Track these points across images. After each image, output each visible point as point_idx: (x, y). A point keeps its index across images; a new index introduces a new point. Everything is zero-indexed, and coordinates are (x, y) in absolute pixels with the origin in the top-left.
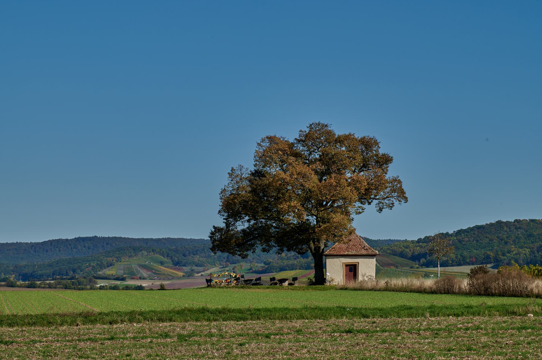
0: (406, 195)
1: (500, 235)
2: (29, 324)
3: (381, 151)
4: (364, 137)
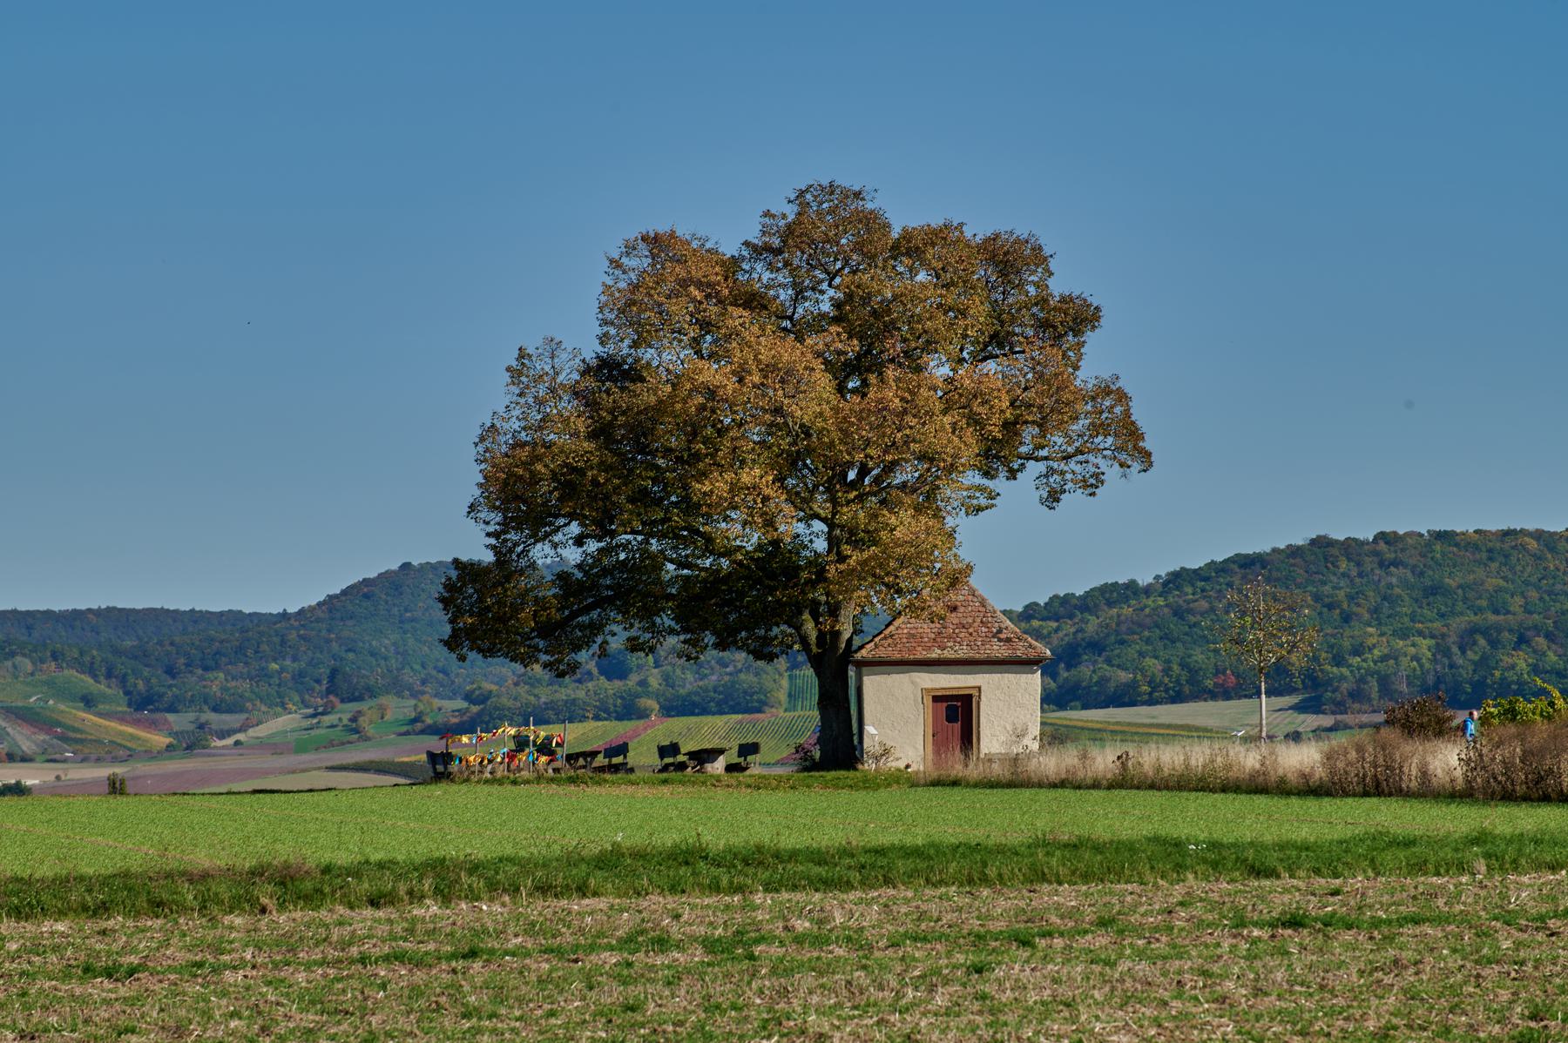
0: (1147, 444)
1: (1327, 589)
2: (85, 908)
3: (1058, 287)
4: (996, 237)
